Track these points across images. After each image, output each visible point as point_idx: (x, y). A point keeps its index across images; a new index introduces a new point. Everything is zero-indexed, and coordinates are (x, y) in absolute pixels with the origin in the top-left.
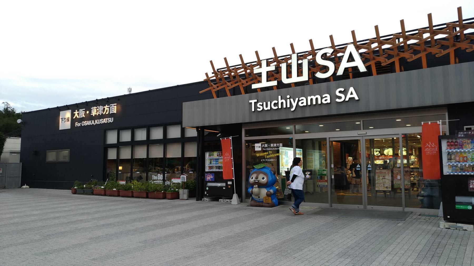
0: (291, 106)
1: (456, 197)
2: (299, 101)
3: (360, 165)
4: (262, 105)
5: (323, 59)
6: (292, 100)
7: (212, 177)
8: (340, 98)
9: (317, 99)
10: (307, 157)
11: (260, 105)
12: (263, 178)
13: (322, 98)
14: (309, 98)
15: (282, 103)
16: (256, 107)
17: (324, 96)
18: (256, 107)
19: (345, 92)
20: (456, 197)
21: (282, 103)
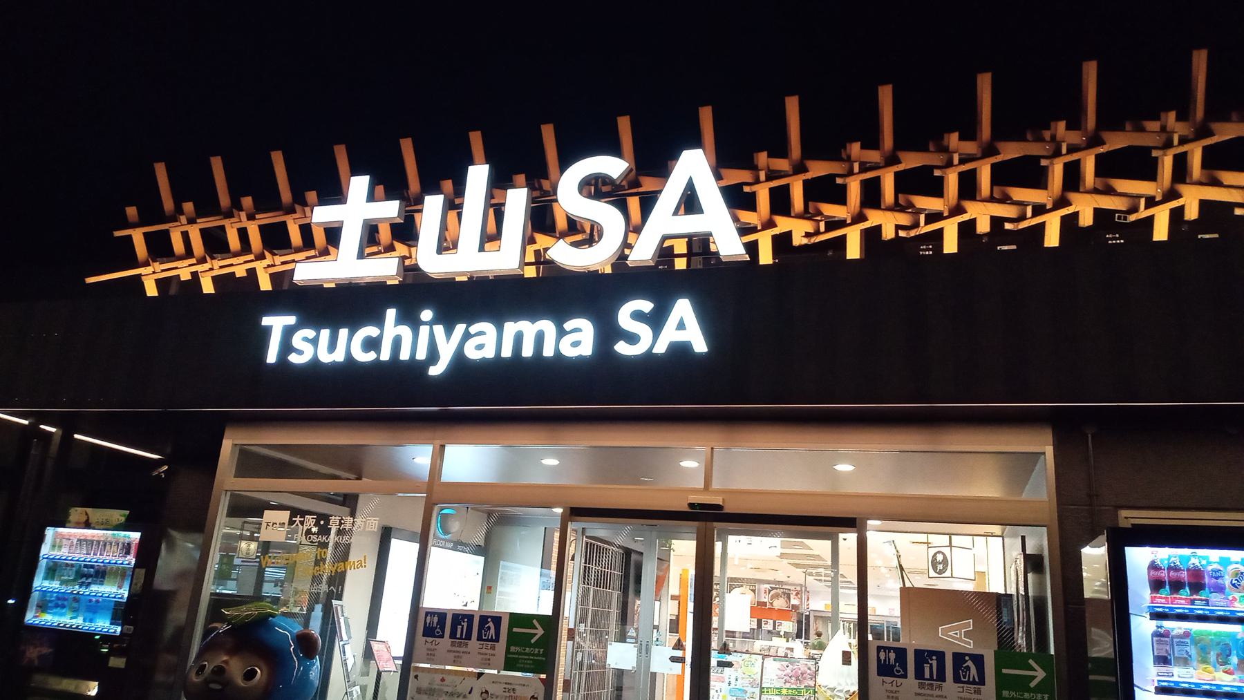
0: (433, 356)
1: (1046, 245)
2: (467, 336)
3: (637, 630)
4: (315, 342)
5: (590, 196)
6: (1032, 684)
7: (46, 650)
8: (632, 339)
9: (540, 338)
10: (499, 589)
11: (306, 339)
12: (250, 675)
13: (561, 333)
14: (511, 328)
15: (397, 342)
16: (287, 347)
17: (568, 325)
18: (287, 347)
19: (656, 320)
20: (1046, 245)
21: (397, 342)
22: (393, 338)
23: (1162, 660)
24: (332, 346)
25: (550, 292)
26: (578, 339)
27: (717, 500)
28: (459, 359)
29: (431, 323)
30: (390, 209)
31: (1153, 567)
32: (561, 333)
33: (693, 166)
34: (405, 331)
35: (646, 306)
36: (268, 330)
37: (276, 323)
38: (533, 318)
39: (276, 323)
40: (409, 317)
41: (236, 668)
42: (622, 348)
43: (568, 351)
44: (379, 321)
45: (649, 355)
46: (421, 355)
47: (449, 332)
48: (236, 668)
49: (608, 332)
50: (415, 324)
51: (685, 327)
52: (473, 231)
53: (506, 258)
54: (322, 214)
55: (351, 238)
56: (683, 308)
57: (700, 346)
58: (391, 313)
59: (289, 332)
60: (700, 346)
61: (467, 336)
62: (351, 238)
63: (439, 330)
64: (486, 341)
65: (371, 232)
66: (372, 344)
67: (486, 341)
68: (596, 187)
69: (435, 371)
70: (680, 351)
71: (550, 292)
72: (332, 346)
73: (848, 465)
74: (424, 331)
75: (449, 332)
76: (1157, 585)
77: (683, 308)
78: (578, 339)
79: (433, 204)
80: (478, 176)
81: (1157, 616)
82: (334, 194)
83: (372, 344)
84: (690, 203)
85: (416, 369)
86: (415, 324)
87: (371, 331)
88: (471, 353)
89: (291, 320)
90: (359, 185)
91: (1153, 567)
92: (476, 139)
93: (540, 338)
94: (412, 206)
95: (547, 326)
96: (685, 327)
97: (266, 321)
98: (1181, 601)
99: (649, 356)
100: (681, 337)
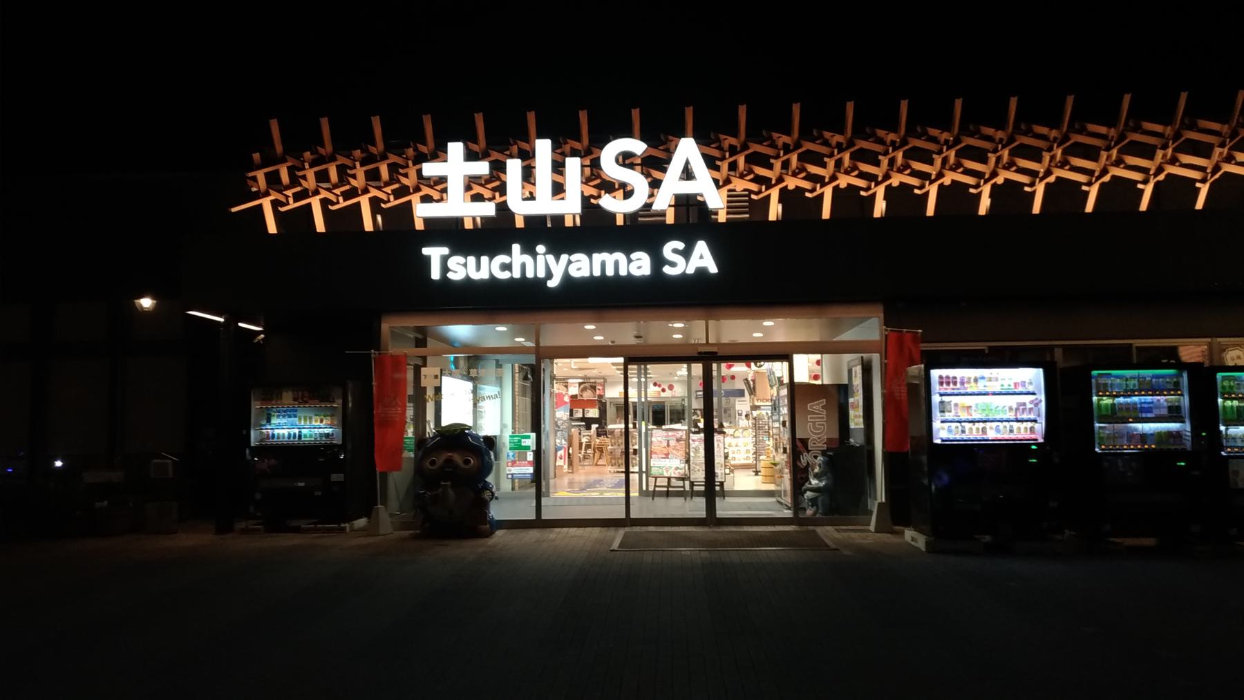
0: (549, 275)
2: (570, 262)
8: (673, 264)
9: (616, 264)
13: (630, 261)
15: (523, 267)
16: (445, 269)
17: (634, 256)
18: (445, 269)
19: (686, 254)
21: (523, 267)
22: (518, 263)
23: (942, 412)
24: (478, 268)
25: (596, 230)
26: (640, 265)
27: (714, 349)
28: (567, 278)
29: (544, 254)
30: (482, 168)
31: (941, 377)
32: (630, 261)
33: (687, 150)
34: (528, 259)
35: (680, 245)
36: (427, 260)
37: (435, 253)
38: (611, 250)
39: (435, 253)
40: (529, 249)
41: (458, 458)
42: (667, 270)
43: (636, 273)
44: (509, 252)
45: (684, 274)
46: (541, 274)
47: (557, 259)
48: (458, 458)
49: (658, 261)
50: (534, 254)
51: (703, 258)
52: (545, 185)
53: (570, 207)
54: (430, 169)
55: (456, 187)
56: (701, 247)
57: (713, 269)
58: (516, 248)
59: (444, 260)
60: (713, 269)
61: (570, 262)
62: (456, 187)
63: (551, 258)
64: (582, 266)
65: (471, 182)
66: (507, 267)
67: (582, 266)
68: (626, 159)
69: (552, 284)
70: (702, 272)
71: (596, 230)
72: (478, 268)
73: (771, 328)
74: (540, 258)
75: (557, 259)
76: (941, 384)
77: (701, 247)
78: (640, 265)
79: (514, 167)
80: (543, 148)
81: (941, 395)
82: (439, 154)
83: (507, 267)
84: (688, 174)
85: (538, 284)
86: (534, 254)
87: (502, 259)
88: (574, 273)
89: (445, 251)
90: (456, 149)
91: (941, 377)
92: (689, 113)
93: (616, 264)
94: (498, 168)
95: (620, 256)
96: (703, 258)
97: (426, 251)
98: (949, 389)
99: (684, 276)
100: (701, 264)
